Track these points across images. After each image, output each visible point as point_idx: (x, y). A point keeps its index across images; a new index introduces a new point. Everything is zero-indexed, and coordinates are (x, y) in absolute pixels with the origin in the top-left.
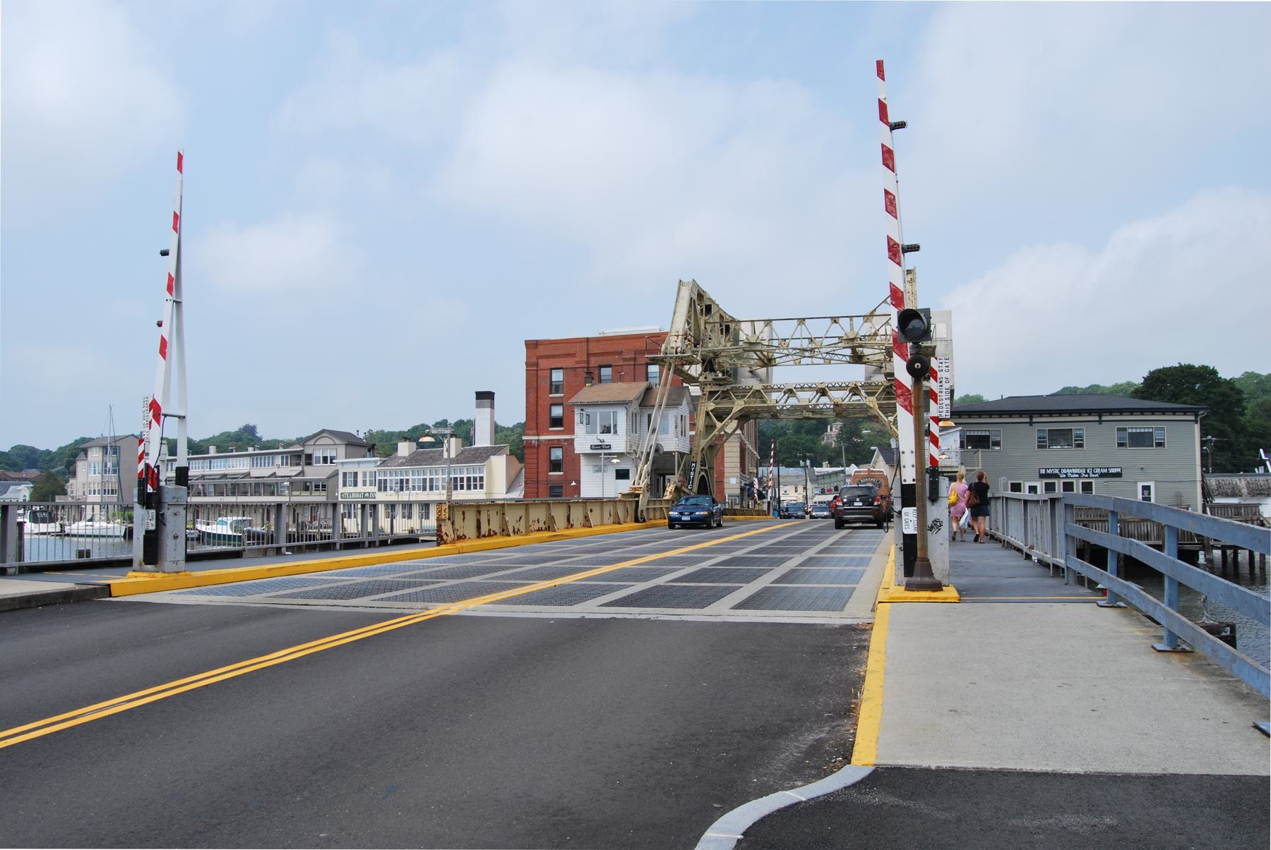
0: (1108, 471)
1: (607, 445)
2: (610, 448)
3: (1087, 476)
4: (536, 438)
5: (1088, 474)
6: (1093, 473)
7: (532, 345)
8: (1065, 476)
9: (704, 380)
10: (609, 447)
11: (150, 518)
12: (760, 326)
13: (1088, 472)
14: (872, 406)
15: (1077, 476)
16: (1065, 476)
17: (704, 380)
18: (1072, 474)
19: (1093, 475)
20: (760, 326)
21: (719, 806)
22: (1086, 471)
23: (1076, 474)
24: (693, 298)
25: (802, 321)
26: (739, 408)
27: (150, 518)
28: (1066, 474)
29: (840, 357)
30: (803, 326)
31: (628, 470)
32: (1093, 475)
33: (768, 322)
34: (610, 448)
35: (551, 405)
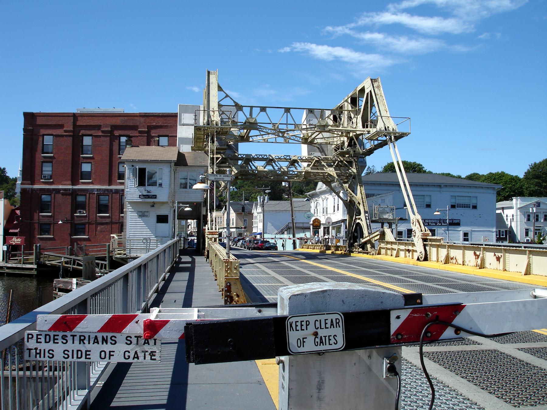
0: (452, 221)
1: (153, 195)
2: (156, 198)
3: (440, 224)
4: (30, 186)
5: (441, 223)
6: (444, 223)
7: (29, 117)
8: (427, 224)
10: (155, 197)
11: (321, 333)
12: (256, 111)
13: (441, 222)
14: (332, 174)
15: (435, 224)
16: (427, 224)
18: (432, 223)
19: (444, 224)
20: (256, 111)
21: (31, 391)
22: (440, 221)
23: (434, 223)
25: (287, 110)
27: (321, 333)
28: (428, 223)
29: (296, 139)
30: (289, 114)
31: (168, 215)
32: (444, 224)
33: (263, 109)
34: (156, 198)
35: (43, 162)
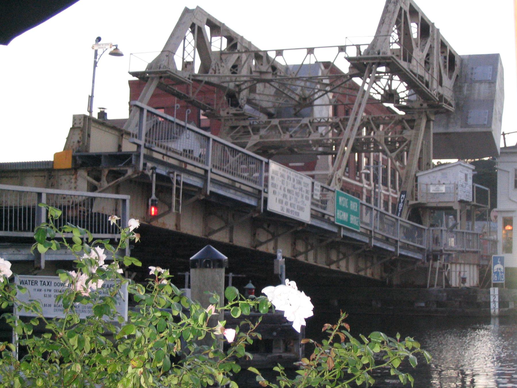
9: (226, 115)
14: (379, 140)
17: (226, 115)
24: (198, 23)
26: (255, 142)
